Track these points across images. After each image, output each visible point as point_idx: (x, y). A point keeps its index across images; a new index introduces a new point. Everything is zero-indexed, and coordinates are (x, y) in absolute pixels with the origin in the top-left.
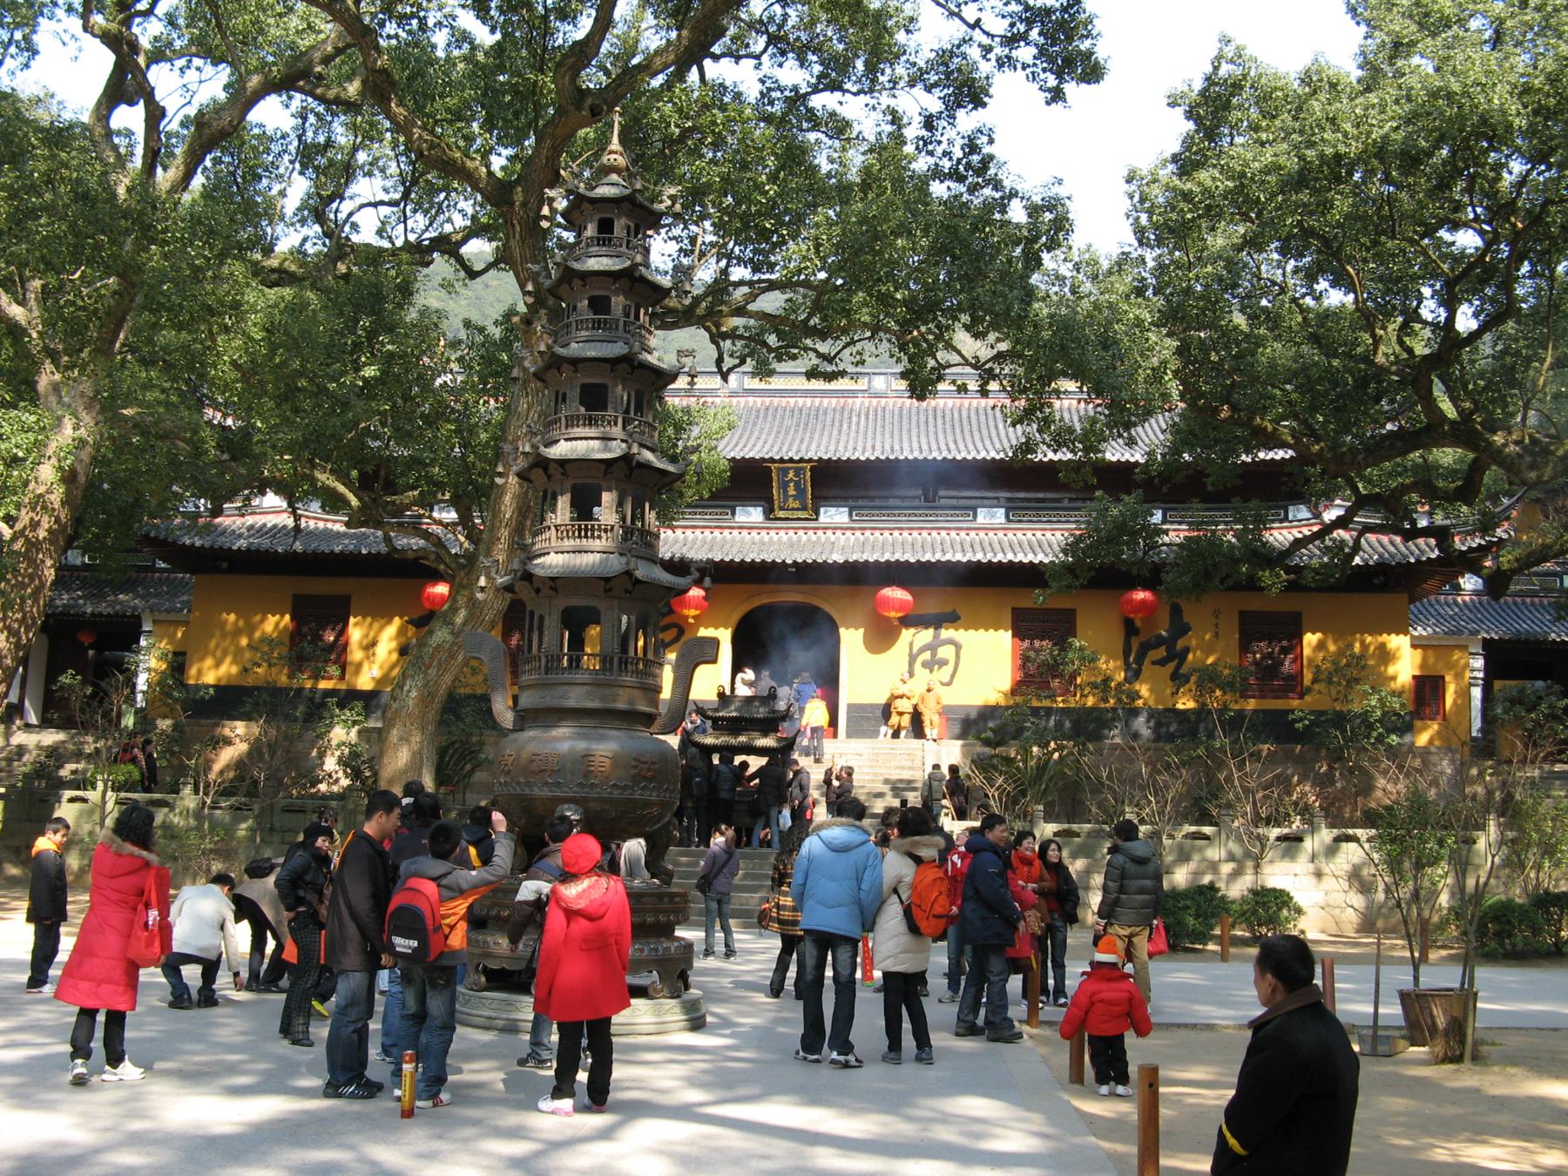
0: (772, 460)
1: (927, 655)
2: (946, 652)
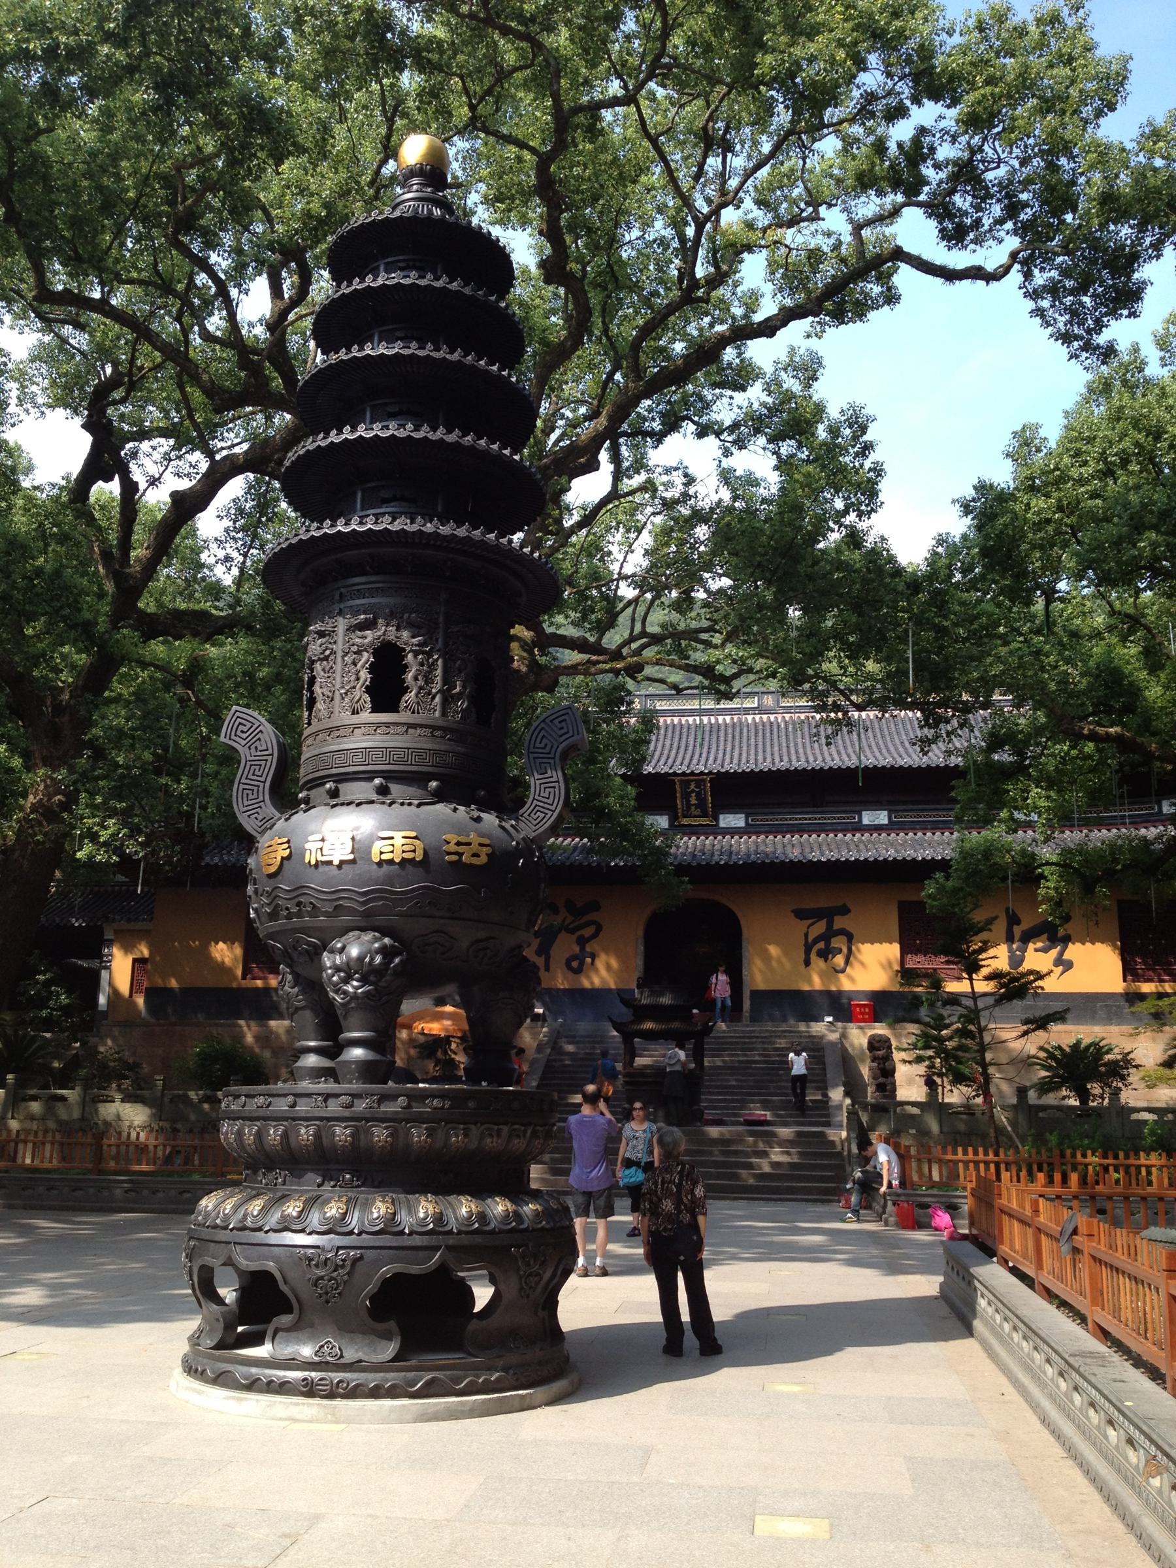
0: (675, 774)
1: (821, 945)
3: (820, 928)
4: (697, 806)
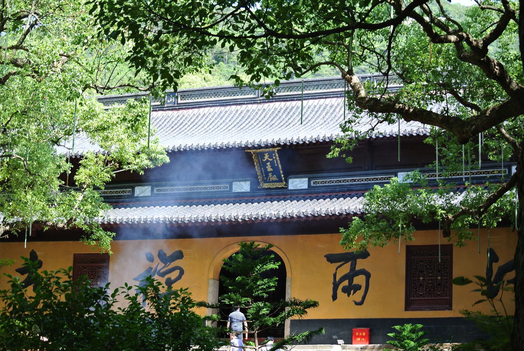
1: (346, 283)
2: (360, 280)
3: (346, 269)
4: (273, 173)
